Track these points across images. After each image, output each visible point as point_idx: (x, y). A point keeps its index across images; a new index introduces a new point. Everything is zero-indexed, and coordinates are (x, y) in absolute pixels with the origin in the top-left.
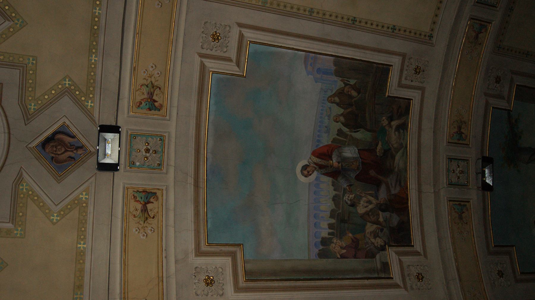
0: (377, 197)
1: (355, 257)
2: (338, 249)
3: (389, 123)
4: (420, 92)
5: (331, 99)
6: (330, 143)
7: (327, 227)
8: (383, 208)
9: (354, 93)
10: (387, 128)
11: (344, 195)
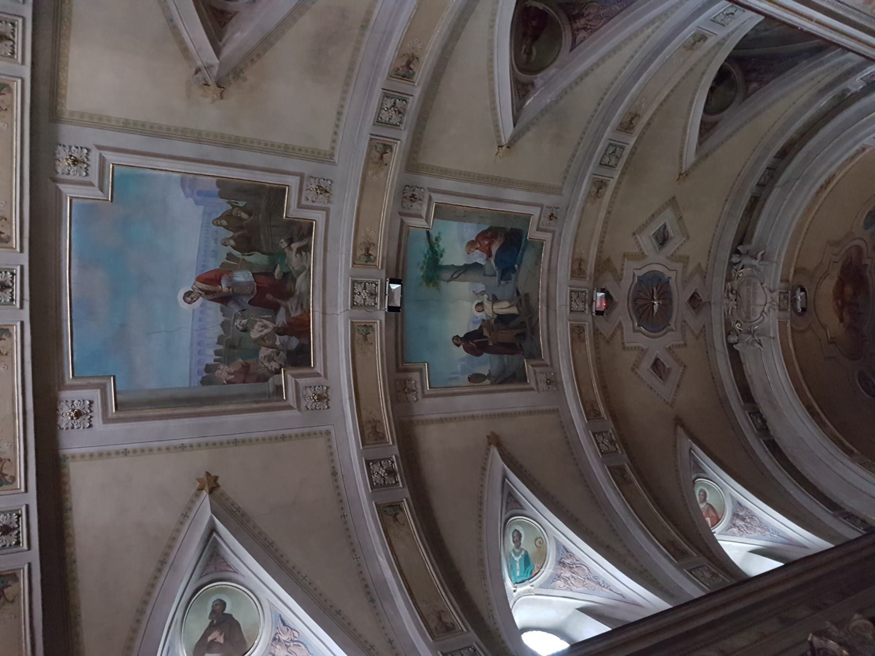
0: (274, 322)
1: (244, 382)
2: (225, 374)
3: (289, 246)
4: (324, 213)
5: (217, 222)
6: (218, 267)
7: (213, 353)
8: (280, 331)
9: (244, 216)
10: (286, 250)
11: (235, 320)
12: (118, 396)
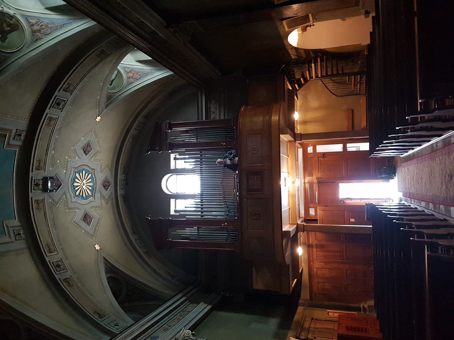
12: (4, 140)
